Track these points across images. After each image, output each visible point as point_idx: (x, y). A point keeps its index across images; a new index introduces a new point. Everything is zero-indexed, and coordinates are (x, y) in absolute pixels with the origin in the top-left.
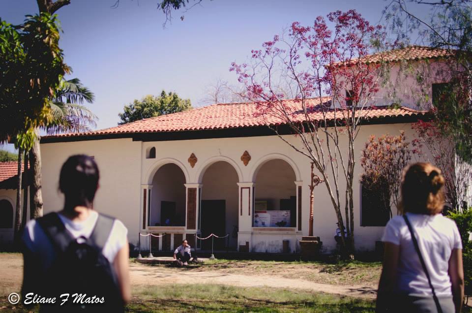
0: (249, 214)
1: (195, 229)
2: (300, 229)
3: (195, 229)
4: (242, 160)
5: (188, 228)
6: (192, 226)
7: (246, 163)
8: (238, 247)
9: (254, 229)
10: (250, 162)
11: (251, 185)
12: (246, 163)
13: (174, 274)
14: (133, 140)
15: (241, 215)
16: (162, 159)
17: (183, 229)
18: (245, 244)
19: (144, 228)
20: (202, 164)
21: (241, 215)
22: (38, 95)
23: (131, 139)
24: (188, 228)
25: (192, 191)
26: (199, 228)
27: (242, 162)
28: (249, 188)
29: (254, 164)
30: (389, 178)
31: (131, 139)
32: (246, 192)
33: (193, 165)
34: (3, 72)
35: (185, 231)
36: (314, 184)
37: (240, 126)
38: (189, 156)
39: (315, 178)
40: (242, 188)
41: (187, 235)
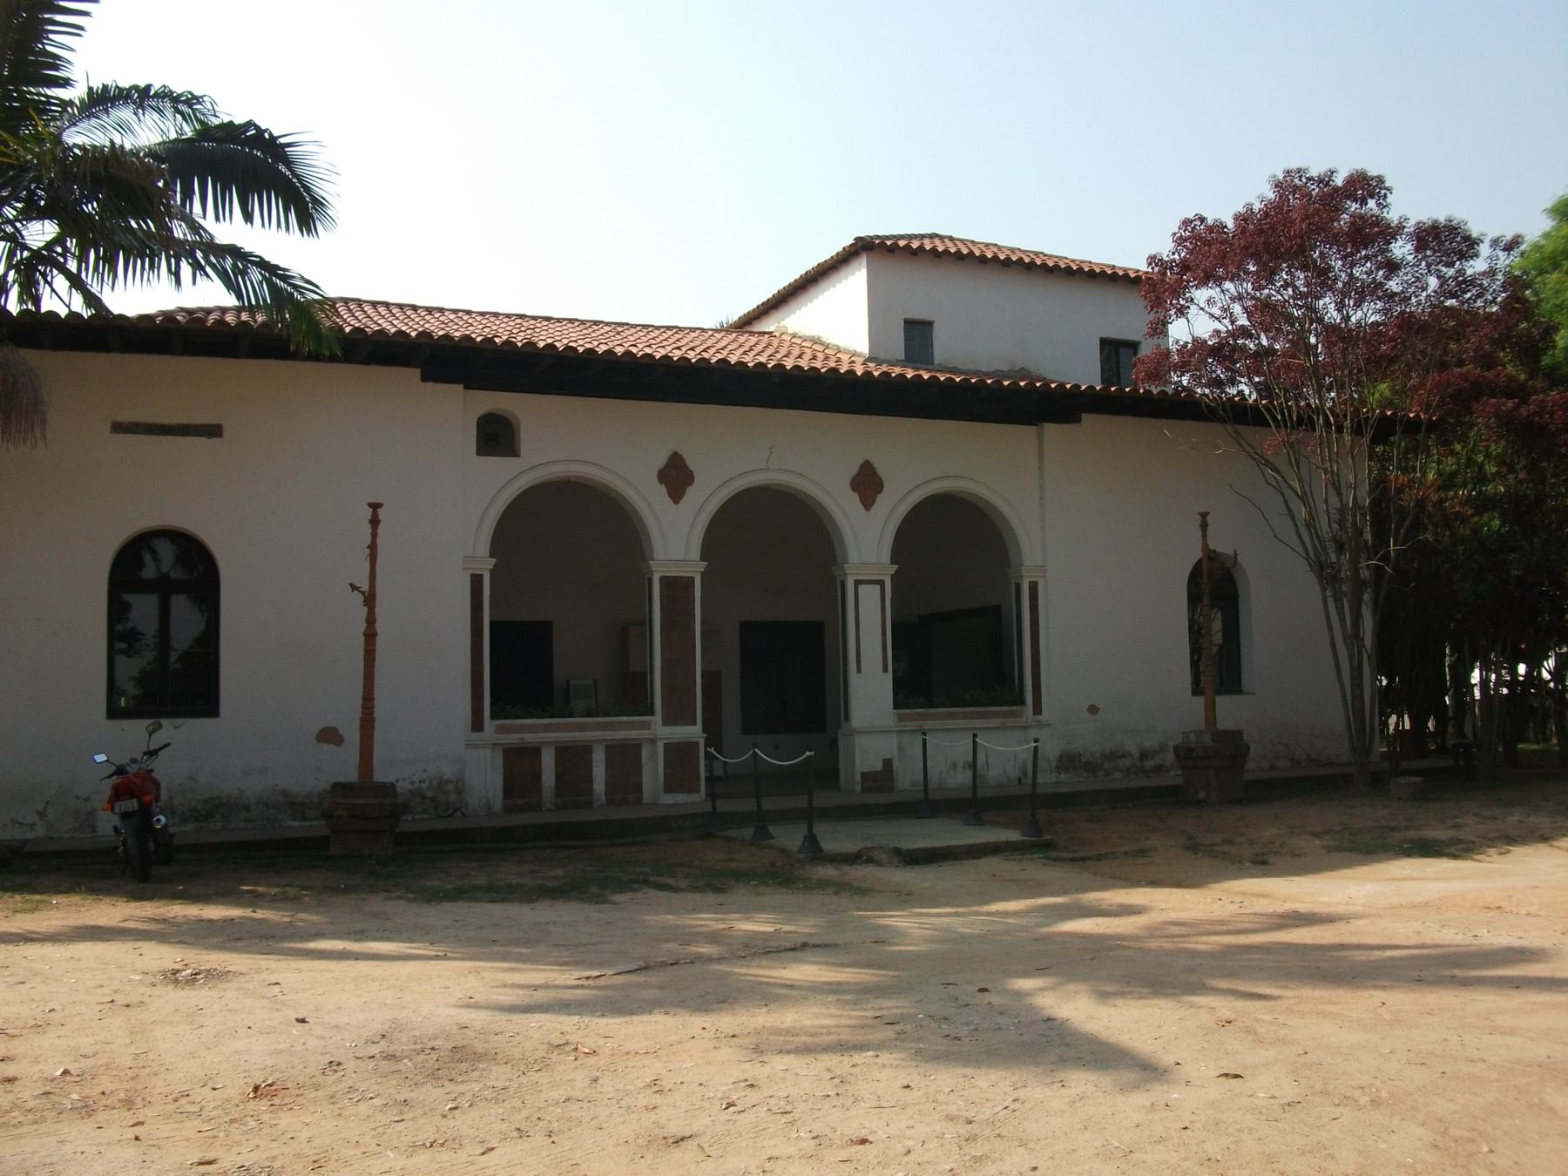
0: (885, 670)
1: (694, 723)
2: (1037, 709)
4: (661, 483)
5: (667, 721)
6: (677, 713)
7: (676, 495)
8: (858, 777)
10: (690, 491)
11: (887, 572)
12: (676, 495)
14: (425, 378)
15: (859, 671)
17: (647, 726)
21: (859, 671)
22: (1476, 491)
23: (462, 386)
24: (667, 721)
25: (677, 588)
27: (856, 496)
28: (881, 583)
29: (704, 499)
30: (1459, 527)
31: (462, 386)
32: (870, 595)
34: (1475, 495)
37: (851, 372)
38: (854, 470)
40: (857, 583)
41: (669, 748)
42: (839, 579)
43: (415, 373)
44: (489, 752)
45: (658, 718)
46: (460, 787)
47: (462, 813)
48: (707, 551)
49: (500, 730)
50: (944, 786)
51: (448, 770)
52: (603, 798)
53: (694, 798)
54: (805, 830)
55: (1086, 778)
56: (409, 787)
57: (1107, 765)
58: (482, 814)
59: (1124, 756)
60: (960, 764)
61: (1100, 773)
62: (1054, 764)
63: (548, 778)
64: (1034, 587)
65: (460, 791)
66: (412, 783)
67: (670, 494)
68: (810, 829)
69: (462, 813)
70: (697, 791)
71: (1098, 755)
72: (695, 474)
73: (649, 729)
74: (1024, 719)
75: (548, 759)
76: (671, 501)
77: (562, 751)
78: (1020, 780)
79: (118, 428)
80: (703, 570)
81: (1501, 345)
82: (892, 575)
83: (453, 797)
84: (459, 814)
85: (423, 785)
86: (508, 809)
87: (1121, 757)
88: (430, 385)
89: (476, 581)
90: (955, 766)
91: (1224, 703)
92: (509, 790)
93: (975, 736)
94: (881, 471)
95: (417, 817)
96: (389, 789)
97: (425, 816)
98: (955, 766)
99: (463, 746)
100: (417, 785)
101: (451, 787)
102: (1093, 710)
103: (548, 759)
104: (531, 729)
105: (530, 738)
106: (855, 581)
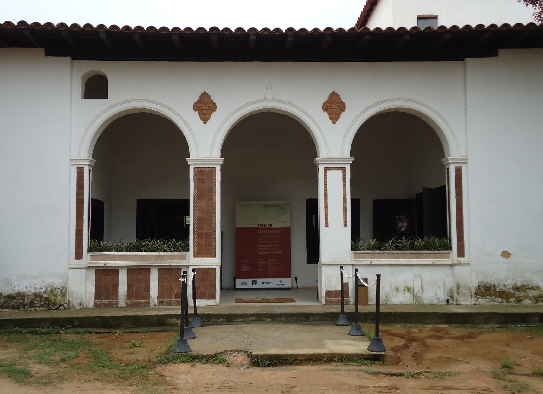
0: (345, 225)
1: (214, 256)
2: (461, 253)
3: (214, 256)
9: (357, 256)
14: (47, 54)
15: (327, 225)
17: (184, 257)
21: (327, 225)
24: (198, 253)
27: (196, 115)
31: (69, 58)
38: (196, 98)
42: (446, 167)
43: (42, 51)
44: (84, 271)
46: (64, 292)
47: (65, 307)
48: (225, 150)
49: (93, 258)
50: (389, 303)
51: (57, 282)
52: (156, 301)
53: (211, 303)
55: (500, 302)
56: (34, 291)
57: (518, 294)
58: (78, 309)
59: (532, 288)
60: (401, 288)
61: (512, 300)
62: (473, 291)
63: (123, 288)
64: (458, 172)
65: (63, 294)
66: (35, 289)
67: (331, 118)
69: (65, 307)
71: (511, 287)
72: (346, 105)
73: (186, 260)
74: (450, 260)
75: (123, 277)
76: (331, 122)
77: (131, 270)
78: (448, 301)
80: (352, 162)
82: (351, 164)
83: (59, 298)
84: (62, 308)
85: (42, 291)
86: (97, 305)
87: (530, 289)
88: (373, 201)
89: (80, 172)
90: (397, 289)
92: (98, 295)
93: (357, 270)
94: (215, 99)
95: (37, 309)
97: (42, 308)
98: (397, 289)
99: (67, 268)
100: (38, 290)
101: (59, 292)
102: (506, 255)
103: (123, 277)
105: (110, 263)
106: (325, 168)
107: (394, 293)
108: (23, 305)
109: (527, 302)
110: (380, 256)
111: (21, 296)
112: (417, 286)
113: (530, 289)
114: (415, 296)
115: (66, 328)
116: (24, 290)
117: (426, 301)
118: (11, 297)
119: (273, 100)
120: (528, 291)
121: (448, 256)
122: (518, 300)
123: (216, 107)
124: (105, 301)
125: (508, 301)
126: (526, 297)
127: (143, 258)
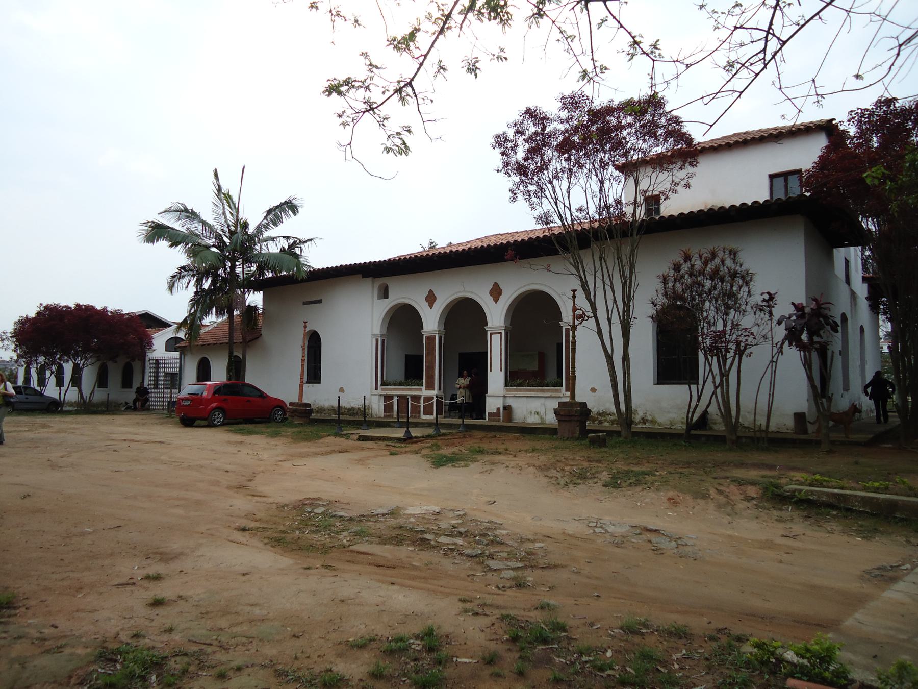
0: (501, 370)
4: (491, 295)
6: (430, 386)
13: (104, 428)
16: (511, 295)
17: (421, 390)
18: (495, 411)
19: (376, 389)
20: (444, 300)
21: (491, 370)
24: (428, 388)
25: (431, 339)
26: (440, 389)
33: (496, 300)
35: (424, 392)
36: (577, 322)
39: (578, 312)
44: (378, 396)
45: (424, 388)
49: (383, 390)
54: (406, 429)
60: (533, 412)
61: (596, 422)
68: (408, 429)
70: (432, 414)
79: (305, 303)
81: (195, 272)
86: (385, 416)
87: (608, 415)
90: (531, 413)
91: (309, 388)
96: (308, 405)
102: (593, 390)
103: (395, 400)
104: (390, 390)
107: (529, 415)
108: (354, 414)
109: (606, 424)
110: (520, 391)
111: (353, 409)
112: (542, 412)
113: (608, 415)
114: (541, 418)
115: (866, 261)
116: (354, 406)
117: (547, 422)
118: (349, 409)
119: (464, 291)
120: (607, 416)
121: (560, 391)
122: (600, 422)
123: (436, 297)
124: (388, 414)
125: (594, 423)
126: (606, 420)
127: (403, 390)
